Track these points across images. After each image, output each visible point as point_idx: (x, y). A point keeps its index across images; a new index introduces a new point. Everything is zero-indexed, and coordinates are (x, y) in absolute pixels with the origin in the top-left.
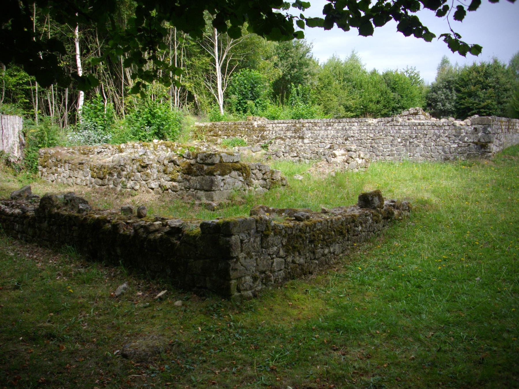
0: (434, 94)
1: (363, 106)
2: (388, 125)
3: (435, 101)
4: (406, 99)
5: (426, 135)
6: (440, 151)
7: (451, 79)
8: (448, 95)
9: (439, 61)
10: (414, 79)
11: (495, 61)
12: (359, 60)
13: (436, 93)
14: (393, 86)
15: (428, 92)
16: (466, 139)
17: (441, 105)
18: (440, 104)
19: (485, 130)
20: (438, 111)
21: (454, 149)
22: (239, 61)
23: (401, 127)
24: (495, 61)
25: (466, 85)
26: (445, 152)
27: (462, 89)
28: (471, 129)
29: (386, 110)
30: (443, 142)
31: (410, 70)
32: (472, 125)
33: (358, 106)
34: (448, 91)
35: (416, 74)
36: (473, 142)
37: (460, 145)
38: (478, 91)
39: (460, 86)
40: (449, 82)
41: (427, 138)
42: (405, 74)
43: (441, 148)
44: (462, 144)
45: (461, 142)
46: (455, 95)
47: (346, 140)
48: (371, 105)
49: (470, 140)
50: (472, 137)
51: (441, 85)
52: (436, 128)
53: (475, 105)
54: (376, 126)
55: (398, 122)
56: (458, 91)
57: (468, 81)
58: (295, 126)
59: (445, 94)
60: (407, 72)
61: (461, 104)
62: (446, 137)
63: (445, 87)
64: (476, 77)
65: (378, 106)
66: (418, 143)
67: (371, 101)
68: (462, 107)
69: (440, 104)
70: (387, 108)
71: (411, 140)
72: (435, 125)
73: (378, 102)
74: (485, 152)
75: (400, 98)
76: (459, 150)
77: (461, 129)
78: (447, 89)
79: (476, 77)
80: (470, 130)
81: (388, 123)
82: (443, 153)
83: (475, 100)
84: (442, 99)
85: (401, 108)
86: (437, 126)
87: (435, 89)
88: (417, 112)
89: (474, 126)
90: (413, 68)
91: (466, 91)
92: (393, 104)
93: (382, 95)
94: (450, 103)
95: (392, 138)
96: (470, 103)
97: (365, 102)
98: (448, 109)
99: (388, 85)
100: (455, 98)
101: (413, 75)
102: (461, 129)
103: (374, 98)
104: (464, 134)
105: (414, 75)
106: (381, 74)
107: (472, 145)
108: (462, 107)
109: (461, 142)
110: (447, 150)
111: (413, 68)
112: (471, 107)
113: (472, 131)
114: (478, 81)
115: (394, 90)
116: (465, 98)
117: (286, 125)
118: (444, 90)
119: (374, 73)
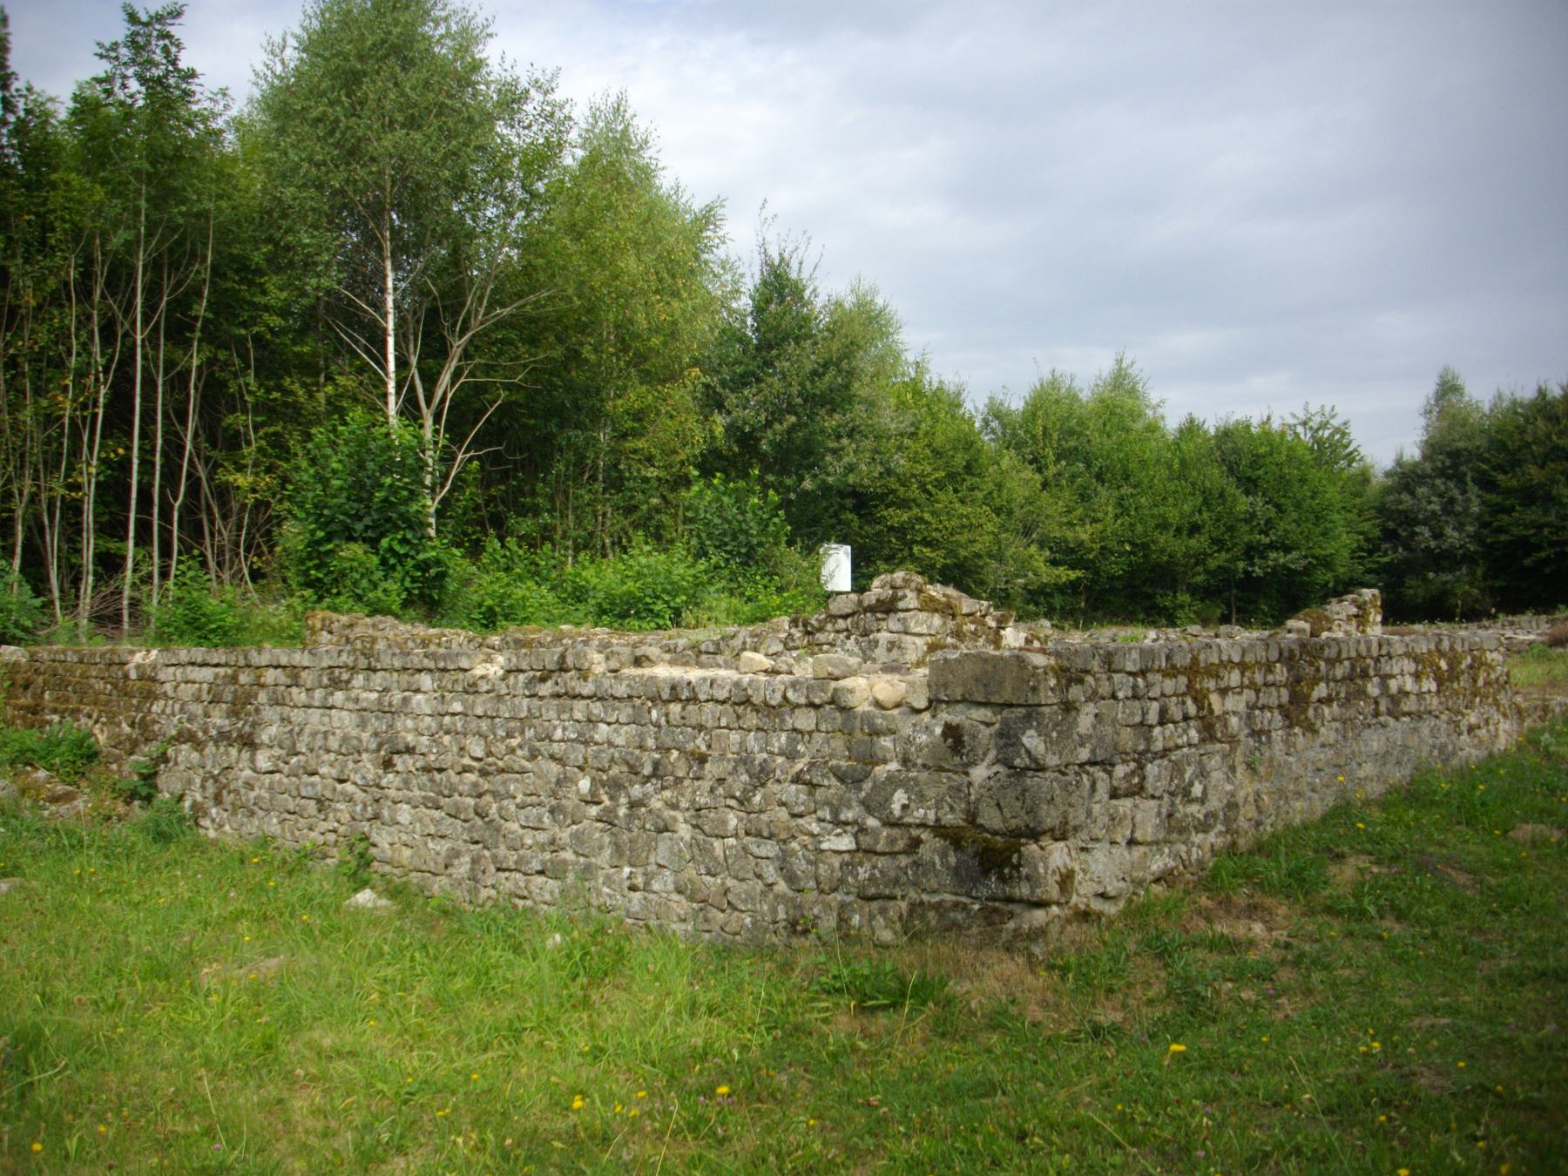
0: (1405, 496)
1: (1132, 544)
2: (545, 689)
3: (1409, 519)
4: (1295, 516)
5: (702, 759)
6: (770, 873)
7: (1461, 445)
8: (1452, 500)
9: (1429, 388)
10: (1330, 449)
11: (707, 218)
12: (1139, 387)
13: (1412, 493)
14: (1249, 473)
15: (1387, 491)
16: (900, 798)
17: (1427, 534)
18: (1425, 531)
19: (1008, 738)
20: (1421, 554)
21: (836, 861)
22: (507, 387)
23: (597, 708)
24: (707, 218)
25: (1513, 463)
26: (791, 879)
27: (1501, 477)
28: (927, 732)
29: (1224, 555)
30: (783, 814)
31: (1317, 419)
32: (933, 704)
33: (1112, 544)
34: (1451, 484)
35: (1337, 430)
36: (939, 829)
37: (866, 841)
38: (1554, 482)
39: (1494, 468)
40: (1455, 455)
41: (706, 785)
42: (1300, 429)
43: (770, 849)
44: (875, 833)
45: (872, 822)
46: (1476, 501)
47: (388, 765)
48: (1163, 539)
49: (919, 814)
50: (931, 793)
51: (1428, 466)
52: (752, 719)
53: (1546, 531)
54: (500, 697)
55: (583, 674)
56: (1487, 484)
57: (1519, 448)
58: (234, 679)
59: (1441, 496)
60: (1304, 424)
61: (1500, 530)
62: (797, 779)
63: (1442, 473)
64: (1548, 437)
65: (1193, 542)
66: (668, 813)
67: (1163, 526)
68: (1503, 538)
69: (1425, 531)
70: (1228, 551)
71: (636, 791)
72: (747, 701)
73: (1195, 529)
74: (1010, 900)
75: (1272, 512)
76: (863, 873)
77: (876, 733)
78: (1449, 478)
79: (1548, 437)
80: (923, 738)
81: (543, 680)
82: (782, 886)
83: (1546, 512)
84: (1434, 512)
85: (1277, 549)
86: (756, 709)
87: (1406, 478)
88: (895, 598)
89: (945, 716)
90: (1327, 410)
91: (1514, 483)
92: (1245, 535)
93: (1206, 502)
94: (1460, 527)
95: (555, 768)
96: (1526, 527)
97: (1139, 528)
98: (1452, 546)
99: (1231, 469)
100: (1475, 509)
101: (1327, 433)
102: (876, 733)
103: (1173, 515)
104: (894, 766)
105: (1332, 435)
106: (1212, 431)
107: (931, 847)
108: (1503, 538)
109: (872, 822)
110: (800, 866)
111: (1327, 410)
112: (1533, 540)
113: (932, 747)
114: (1556, 448)
115: (1250, 485)
116: (1513, 509)
117: (207, 674)
118: (1438, 482)
119: (1191, 429)
